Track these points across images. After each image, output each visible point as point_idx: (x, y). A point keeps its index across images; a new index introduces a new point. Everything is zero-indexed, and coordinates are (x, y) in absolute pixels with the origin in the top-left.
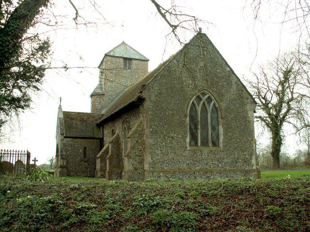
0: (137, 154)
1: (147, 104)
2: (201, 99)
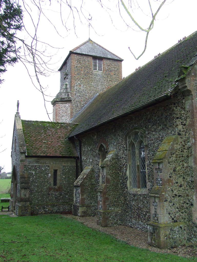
0: (175, 192)
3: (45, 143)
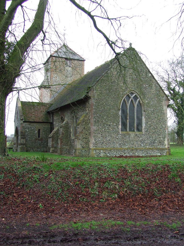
0: (84, 137)
1: (92, 101)
2: (130, 98)
3: (34, 114)
